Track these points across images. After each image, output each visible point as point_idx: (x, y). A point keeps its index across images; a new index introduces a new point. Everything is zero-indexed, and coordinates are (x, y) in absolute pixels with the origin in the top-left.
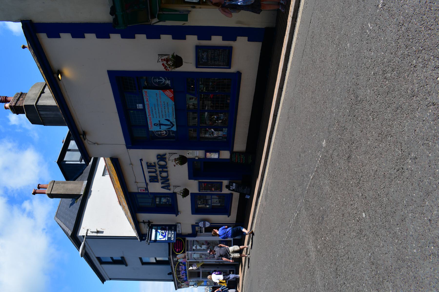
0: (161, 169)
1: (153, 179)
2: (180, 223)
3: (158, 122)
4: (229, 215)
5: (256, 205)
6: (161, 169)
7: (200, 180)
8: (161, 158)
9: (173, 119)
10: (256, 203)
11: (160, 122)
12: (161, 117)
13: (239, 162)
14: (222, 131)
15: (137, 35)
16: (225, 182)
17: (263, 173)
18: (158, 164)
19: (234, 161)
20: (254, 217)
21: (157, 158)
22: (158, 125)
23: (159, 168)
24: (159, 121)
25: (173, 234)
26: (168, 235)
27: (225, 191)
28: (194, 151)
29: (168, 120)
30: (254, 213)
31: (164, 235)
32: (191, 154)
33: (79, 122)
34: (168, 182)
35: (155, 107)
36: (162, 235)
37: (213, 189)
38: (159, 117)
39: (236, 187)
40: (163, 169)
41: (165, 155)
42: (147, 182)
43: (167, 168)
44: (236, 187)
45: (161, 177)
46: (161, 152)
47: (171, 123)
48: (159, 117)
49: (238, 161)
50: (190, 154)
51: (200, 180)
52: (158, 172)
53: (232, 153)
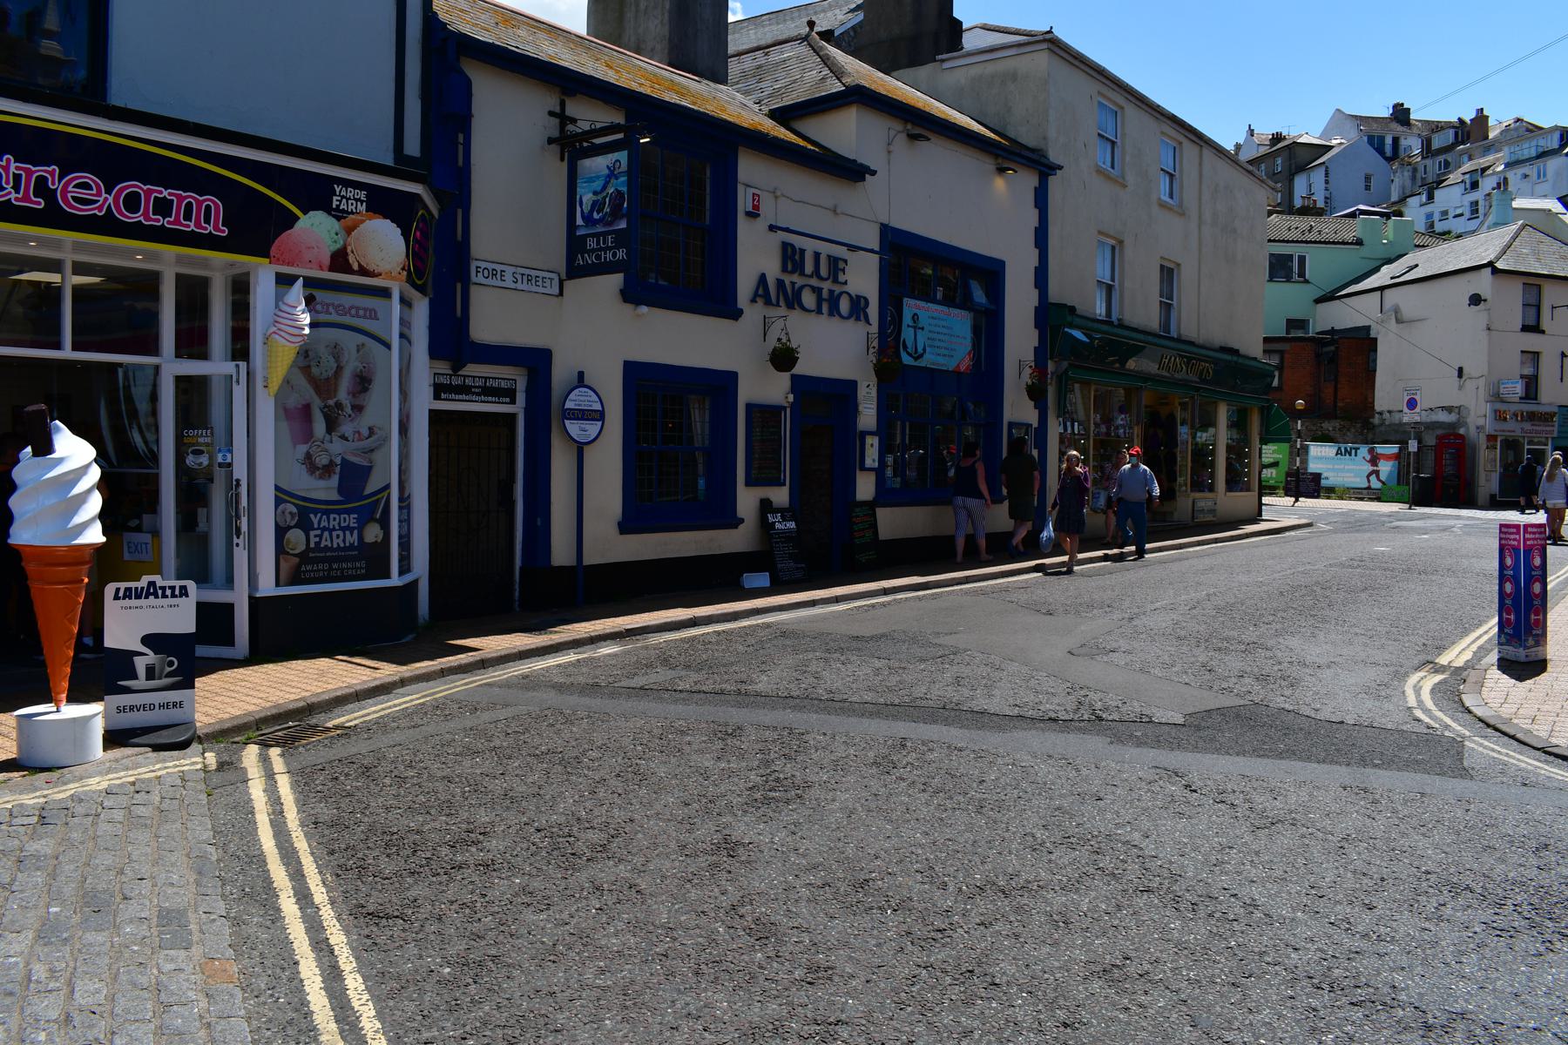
0: (825, 294)
1: (791, 257)
2: (561, 294)
3: (920, 325)
4: (628, 525)
5: (886, 592)
6: (825, 294)
7: (788, 410)
8: (858, 307)
9: (929, 360)
10: (894, 587)
11: (920, 328)
12: (931, 335)
13: (856, 528)
14: (895, 475)
15: (415, 155)
16: (780, 496)
17: (976, 578)
18: (841, 293)
19: (854, 514)
20: (837, 602)
21: (862, 297)
22: (915, 322)
23: (831, 292)
24: (923, 329)
25: (598, 257)
26: (593, 235)
27: (747, 500)
28: (875, 403)
29: (924, 350)
30: (666, 623)
31: (596, 216)
32: (868, 393)
33: (978, 159)
34: (782, 303)
35: (948, 328)
36: (594, 203)
37: (1238, 479)
38: (930, 331)
39: (782, 533)
40: (825, 300)
41: (868, 322)
42: (779, 232)
43: (831, 314)
44: (784, 532)
45: (803, 287)
46: (873, 311)
47: (921, 356)
48: (930, 331)
49: (858, 523)
50: (868, 390)
51: (788, 410)
52: (814, 282)
53: (871, 506)
